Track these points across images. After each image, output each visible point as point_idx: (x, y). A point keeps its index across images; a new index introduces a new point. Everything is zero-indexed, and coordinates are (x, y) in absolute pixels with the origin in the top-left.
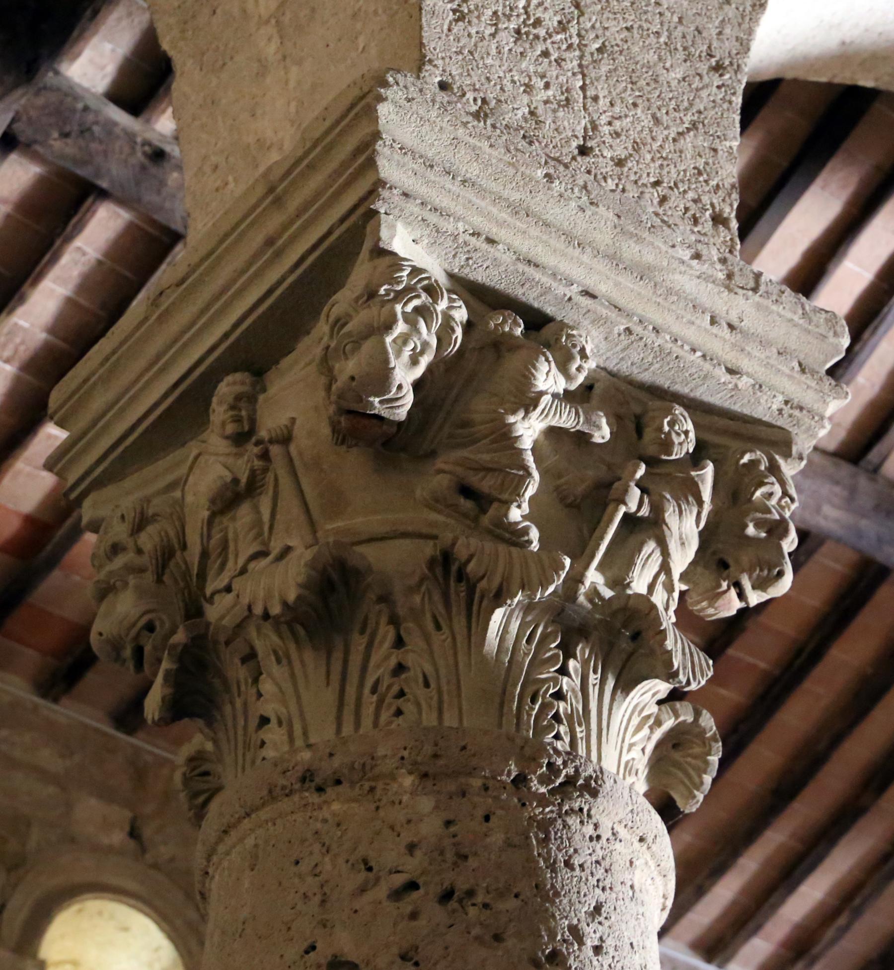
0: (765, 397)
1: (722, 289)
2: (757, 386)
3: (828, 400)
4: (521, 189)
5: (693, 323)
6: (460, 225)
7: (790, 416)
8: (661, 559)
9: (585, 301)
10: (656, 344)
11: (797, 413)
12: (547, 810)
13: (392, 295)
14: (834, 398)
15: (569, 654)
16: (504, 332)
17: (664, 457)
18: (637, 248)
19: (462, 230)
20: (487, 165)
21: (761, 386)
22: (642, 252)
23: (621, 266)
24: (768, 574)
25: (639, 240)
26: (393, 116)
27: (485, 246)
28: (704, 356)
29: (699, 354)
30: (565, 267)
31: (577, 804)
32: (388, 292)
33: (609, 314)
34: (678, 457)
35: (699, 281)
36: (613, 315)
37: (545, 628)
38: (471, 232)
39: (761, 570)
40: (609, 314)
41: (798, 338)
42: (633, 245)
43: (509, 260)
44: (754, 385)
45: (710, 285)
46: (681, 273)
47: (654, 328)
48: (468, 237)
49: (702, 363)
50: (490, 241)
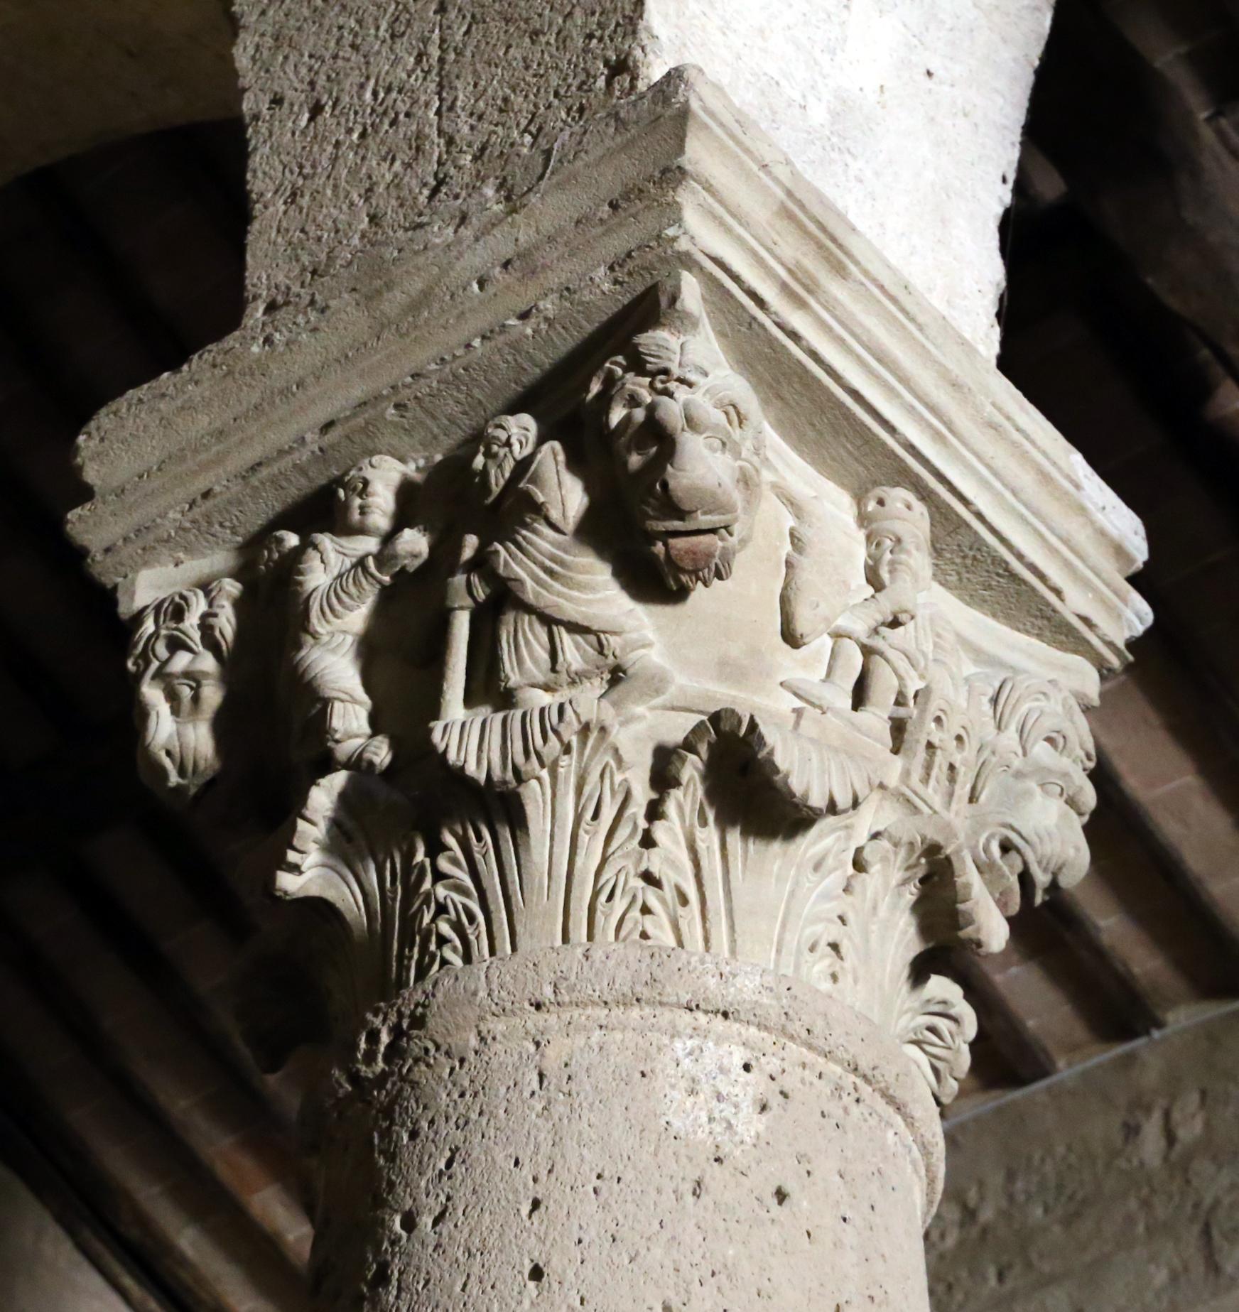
0: (586, 292)
1: (510, 219)
2: (566, 293)
3: (670, 199)
4: (254, 383)
5: (463, 313)
6: (171, 515)
7: (630, 274)
8: (534, 617)
9: (334, 435)
10: (434, 384)
11: (630, 265)
12: (389, 1086)
13: (140, 662)
14: (674, 190)
15: (437, 847)
16: (275, 562)
17: (491, 499)
18: (398, 294)
19: (179, 516)
20: (208, 404)
21: (568, 289)
22: (405, 290)
23: (775, 125)
24: (657, 499)
25: (389, 286)
26: (104, 470)
27: (210, 503)
28: (484, 337)
29: (477, 342)
30: (283, 436)
31: (417, 1050)
32: (135, 663)
33: (366, 416)
34: (502, 482)
35: (481, 243)
36: (370, 413)
37: (401, 850)
38: (187, 506)
39: (648, 505)
40: (366, 416)
41: (630, 158)
42: (390, 295)
43: (239, 488)
44: (561, 296)
45: (495, 231)
46: (458, 259)
47: (412, 376)
48: (190, 515)
49: (493, 343)
50: (206, 495)
